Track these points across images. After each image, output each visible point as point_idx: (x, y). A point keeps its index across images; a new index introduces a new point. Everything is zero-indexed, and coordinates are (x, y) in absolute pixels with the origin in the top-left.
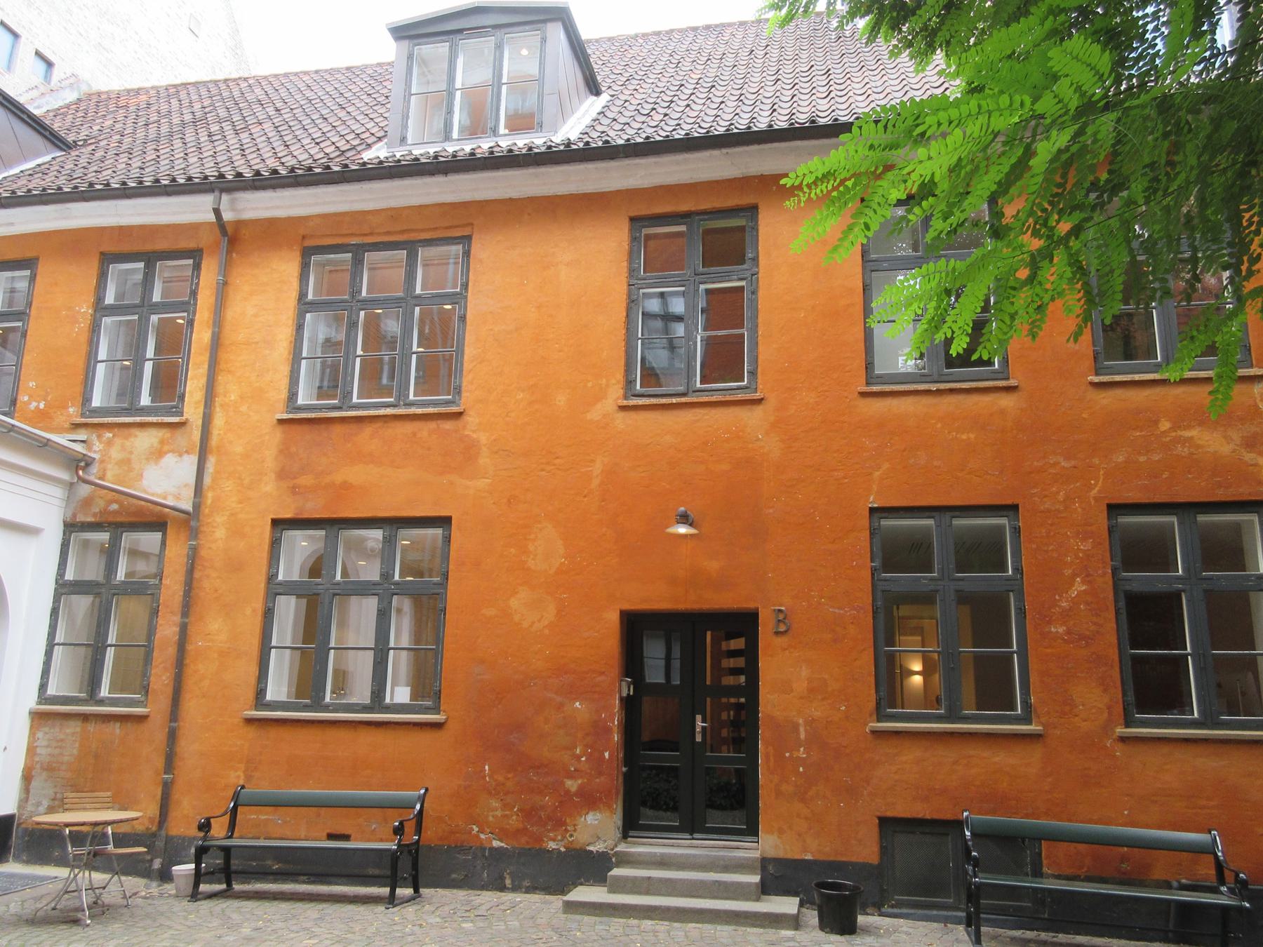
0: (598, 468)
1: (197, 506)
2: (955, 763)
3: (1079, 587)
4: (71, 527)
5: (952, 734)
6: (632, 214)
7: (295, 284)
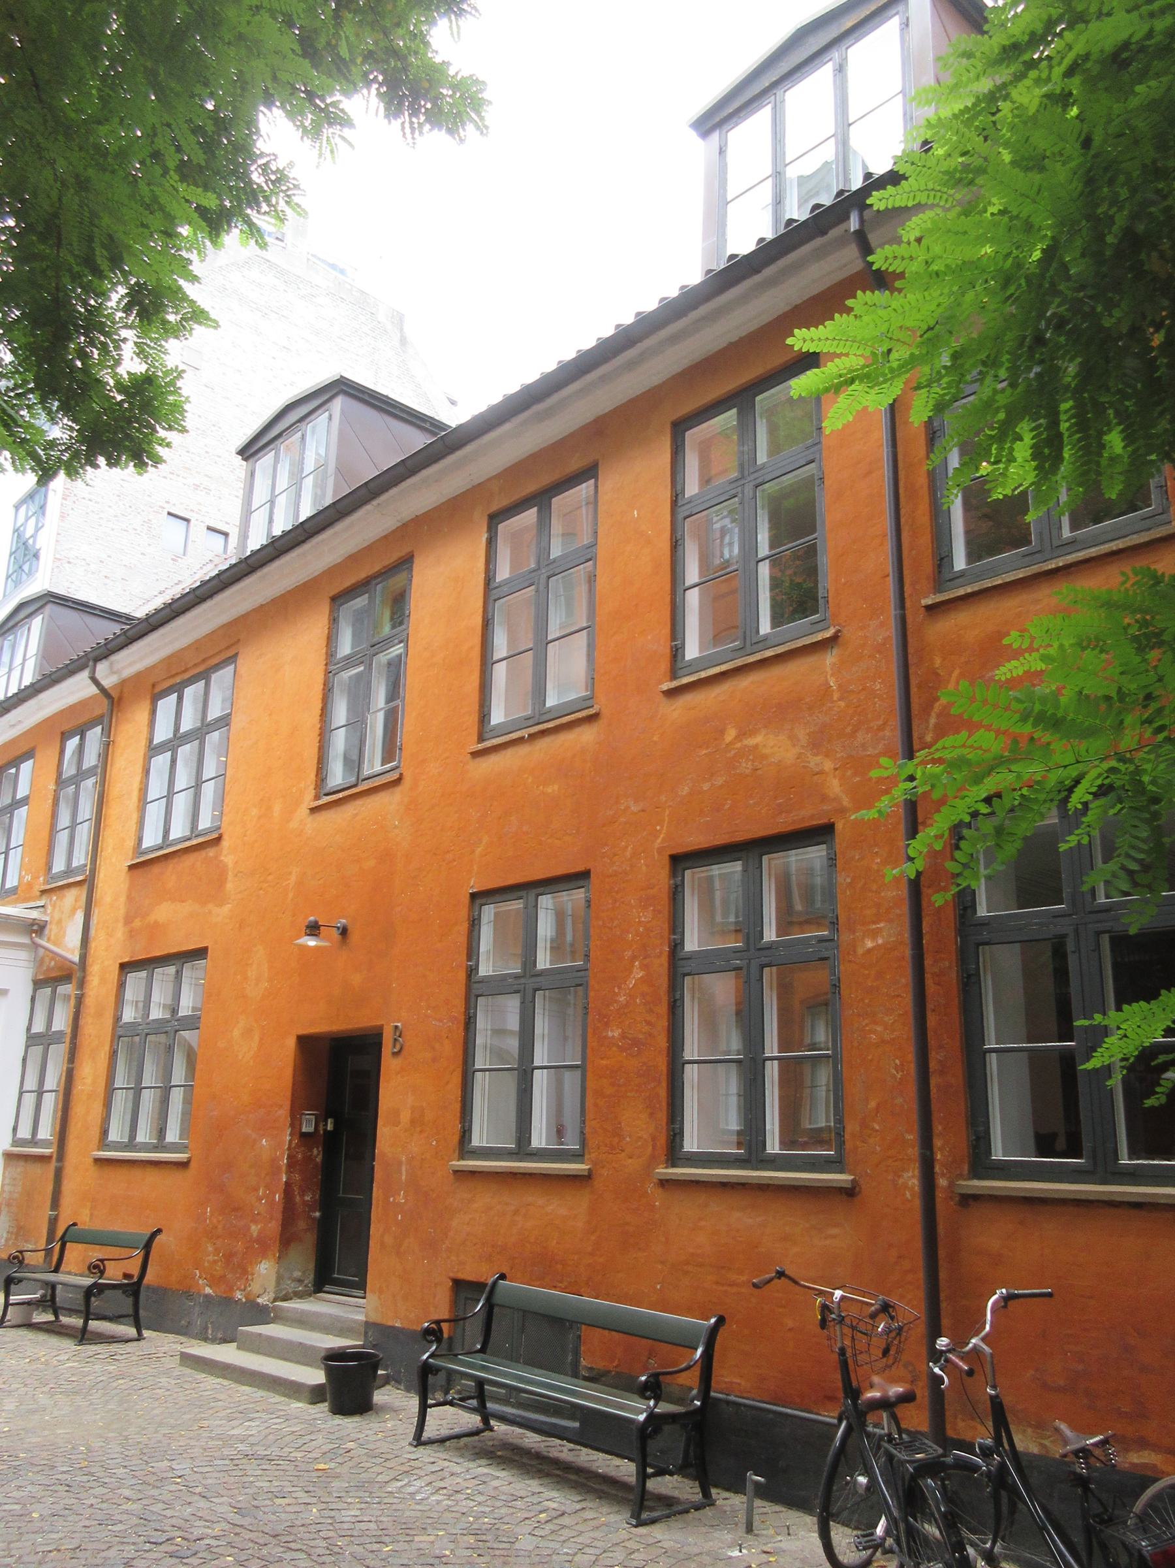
1: (84, 957)
2: (516, 1212)
3: (638, 974)
4: (38, 984)
5: (513, 1175)
6: (332, 594)
7: (145, 730)
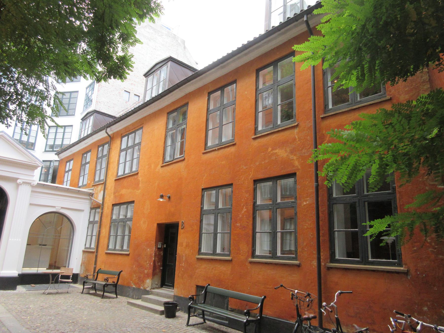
0: (156, 184)
1: (103, 202)
2: (213, 269)
4: (91, 209)
5: (212, 260)
7: (119, 145)
